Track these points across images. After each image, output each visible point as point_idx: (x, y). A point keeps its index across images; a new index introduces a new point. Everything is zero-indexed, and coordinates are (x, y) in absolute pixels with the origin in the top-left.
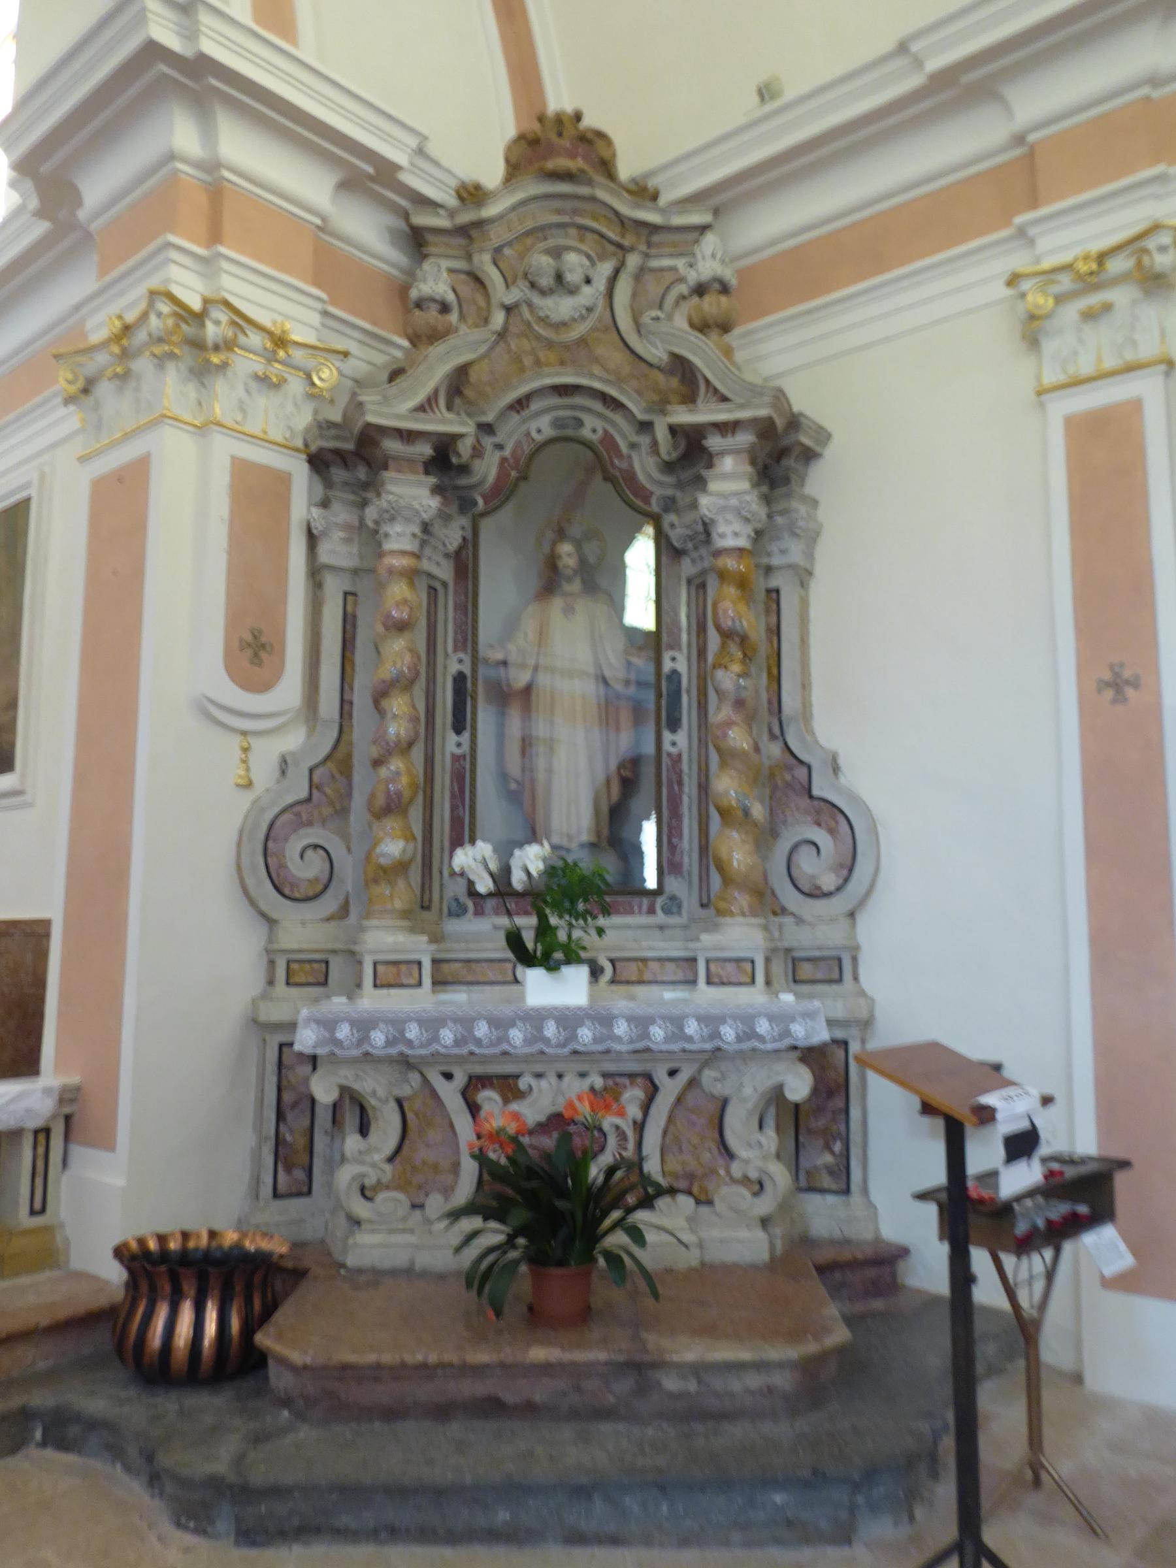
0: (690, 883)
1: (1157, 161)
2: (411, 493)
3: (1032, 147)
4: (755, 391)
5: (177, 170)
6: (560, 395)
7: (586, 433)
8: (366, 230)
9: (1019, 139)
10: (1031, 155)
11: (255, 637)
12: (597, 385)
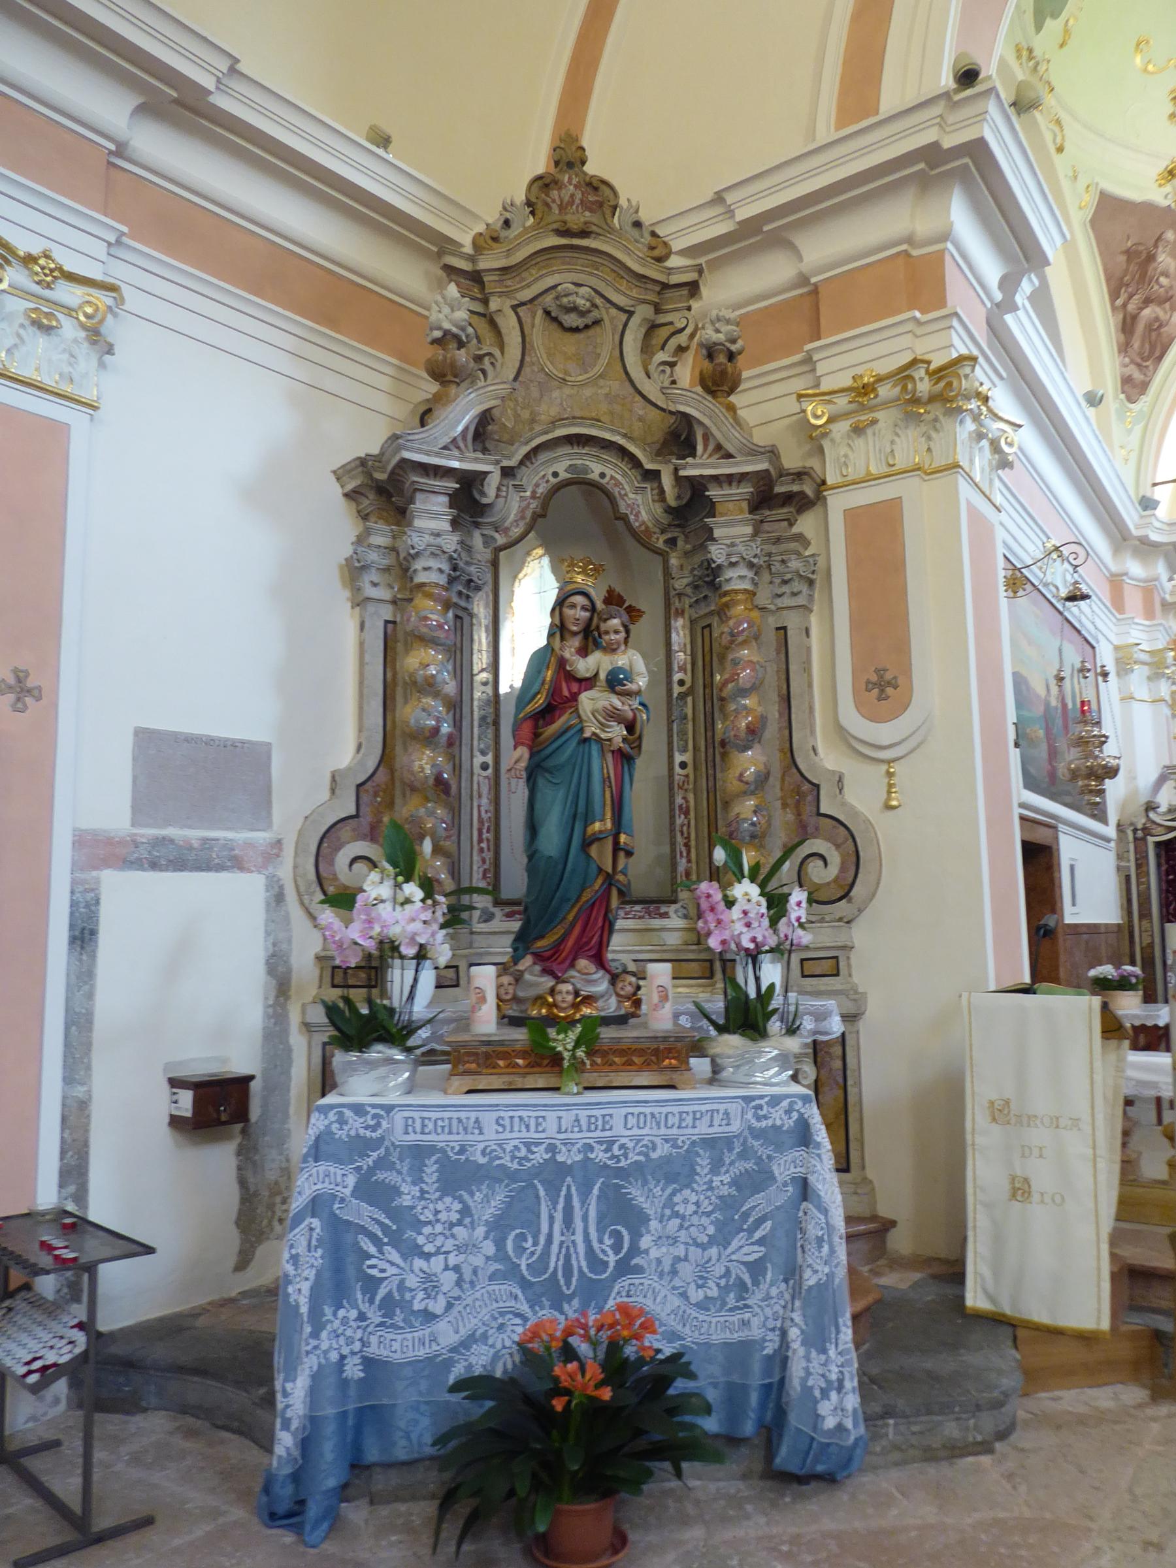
0: (677, 951)
1: (910, 309)
2: (432, 516)
3: (815, 285)
4: (754, 452)
5: (947, 249)
6: (572, 444)
7: (563, 475)
8: (734, 293)
9: (803, 280)
10: (815, 291)
11: (19, 680)
12: (607, 436)
